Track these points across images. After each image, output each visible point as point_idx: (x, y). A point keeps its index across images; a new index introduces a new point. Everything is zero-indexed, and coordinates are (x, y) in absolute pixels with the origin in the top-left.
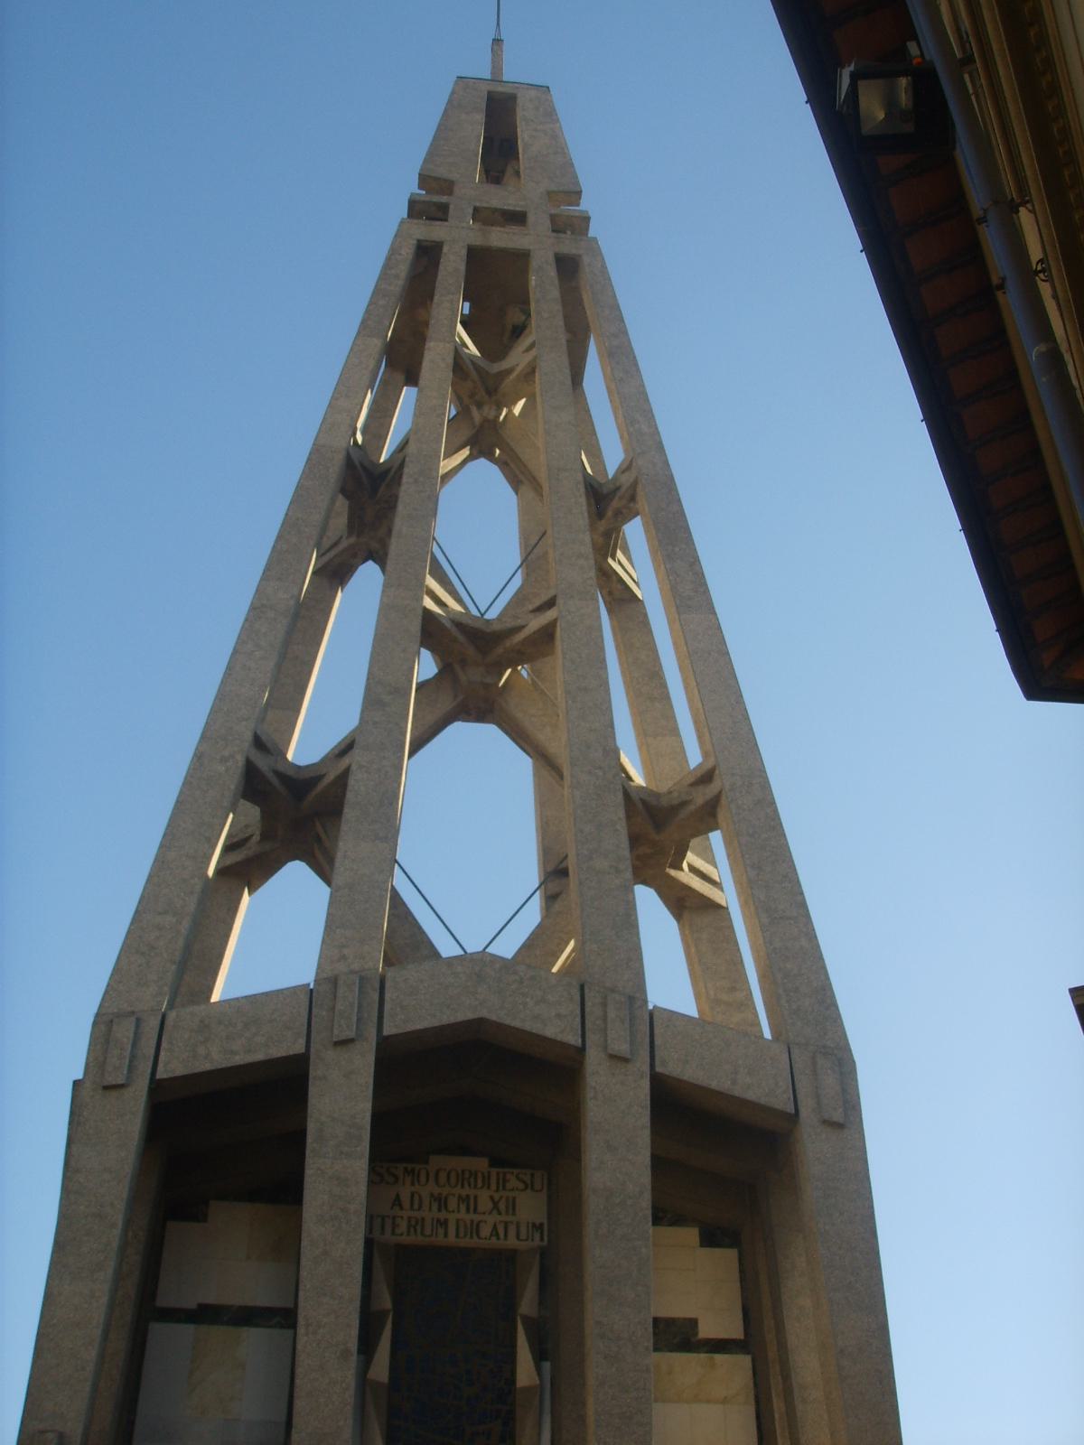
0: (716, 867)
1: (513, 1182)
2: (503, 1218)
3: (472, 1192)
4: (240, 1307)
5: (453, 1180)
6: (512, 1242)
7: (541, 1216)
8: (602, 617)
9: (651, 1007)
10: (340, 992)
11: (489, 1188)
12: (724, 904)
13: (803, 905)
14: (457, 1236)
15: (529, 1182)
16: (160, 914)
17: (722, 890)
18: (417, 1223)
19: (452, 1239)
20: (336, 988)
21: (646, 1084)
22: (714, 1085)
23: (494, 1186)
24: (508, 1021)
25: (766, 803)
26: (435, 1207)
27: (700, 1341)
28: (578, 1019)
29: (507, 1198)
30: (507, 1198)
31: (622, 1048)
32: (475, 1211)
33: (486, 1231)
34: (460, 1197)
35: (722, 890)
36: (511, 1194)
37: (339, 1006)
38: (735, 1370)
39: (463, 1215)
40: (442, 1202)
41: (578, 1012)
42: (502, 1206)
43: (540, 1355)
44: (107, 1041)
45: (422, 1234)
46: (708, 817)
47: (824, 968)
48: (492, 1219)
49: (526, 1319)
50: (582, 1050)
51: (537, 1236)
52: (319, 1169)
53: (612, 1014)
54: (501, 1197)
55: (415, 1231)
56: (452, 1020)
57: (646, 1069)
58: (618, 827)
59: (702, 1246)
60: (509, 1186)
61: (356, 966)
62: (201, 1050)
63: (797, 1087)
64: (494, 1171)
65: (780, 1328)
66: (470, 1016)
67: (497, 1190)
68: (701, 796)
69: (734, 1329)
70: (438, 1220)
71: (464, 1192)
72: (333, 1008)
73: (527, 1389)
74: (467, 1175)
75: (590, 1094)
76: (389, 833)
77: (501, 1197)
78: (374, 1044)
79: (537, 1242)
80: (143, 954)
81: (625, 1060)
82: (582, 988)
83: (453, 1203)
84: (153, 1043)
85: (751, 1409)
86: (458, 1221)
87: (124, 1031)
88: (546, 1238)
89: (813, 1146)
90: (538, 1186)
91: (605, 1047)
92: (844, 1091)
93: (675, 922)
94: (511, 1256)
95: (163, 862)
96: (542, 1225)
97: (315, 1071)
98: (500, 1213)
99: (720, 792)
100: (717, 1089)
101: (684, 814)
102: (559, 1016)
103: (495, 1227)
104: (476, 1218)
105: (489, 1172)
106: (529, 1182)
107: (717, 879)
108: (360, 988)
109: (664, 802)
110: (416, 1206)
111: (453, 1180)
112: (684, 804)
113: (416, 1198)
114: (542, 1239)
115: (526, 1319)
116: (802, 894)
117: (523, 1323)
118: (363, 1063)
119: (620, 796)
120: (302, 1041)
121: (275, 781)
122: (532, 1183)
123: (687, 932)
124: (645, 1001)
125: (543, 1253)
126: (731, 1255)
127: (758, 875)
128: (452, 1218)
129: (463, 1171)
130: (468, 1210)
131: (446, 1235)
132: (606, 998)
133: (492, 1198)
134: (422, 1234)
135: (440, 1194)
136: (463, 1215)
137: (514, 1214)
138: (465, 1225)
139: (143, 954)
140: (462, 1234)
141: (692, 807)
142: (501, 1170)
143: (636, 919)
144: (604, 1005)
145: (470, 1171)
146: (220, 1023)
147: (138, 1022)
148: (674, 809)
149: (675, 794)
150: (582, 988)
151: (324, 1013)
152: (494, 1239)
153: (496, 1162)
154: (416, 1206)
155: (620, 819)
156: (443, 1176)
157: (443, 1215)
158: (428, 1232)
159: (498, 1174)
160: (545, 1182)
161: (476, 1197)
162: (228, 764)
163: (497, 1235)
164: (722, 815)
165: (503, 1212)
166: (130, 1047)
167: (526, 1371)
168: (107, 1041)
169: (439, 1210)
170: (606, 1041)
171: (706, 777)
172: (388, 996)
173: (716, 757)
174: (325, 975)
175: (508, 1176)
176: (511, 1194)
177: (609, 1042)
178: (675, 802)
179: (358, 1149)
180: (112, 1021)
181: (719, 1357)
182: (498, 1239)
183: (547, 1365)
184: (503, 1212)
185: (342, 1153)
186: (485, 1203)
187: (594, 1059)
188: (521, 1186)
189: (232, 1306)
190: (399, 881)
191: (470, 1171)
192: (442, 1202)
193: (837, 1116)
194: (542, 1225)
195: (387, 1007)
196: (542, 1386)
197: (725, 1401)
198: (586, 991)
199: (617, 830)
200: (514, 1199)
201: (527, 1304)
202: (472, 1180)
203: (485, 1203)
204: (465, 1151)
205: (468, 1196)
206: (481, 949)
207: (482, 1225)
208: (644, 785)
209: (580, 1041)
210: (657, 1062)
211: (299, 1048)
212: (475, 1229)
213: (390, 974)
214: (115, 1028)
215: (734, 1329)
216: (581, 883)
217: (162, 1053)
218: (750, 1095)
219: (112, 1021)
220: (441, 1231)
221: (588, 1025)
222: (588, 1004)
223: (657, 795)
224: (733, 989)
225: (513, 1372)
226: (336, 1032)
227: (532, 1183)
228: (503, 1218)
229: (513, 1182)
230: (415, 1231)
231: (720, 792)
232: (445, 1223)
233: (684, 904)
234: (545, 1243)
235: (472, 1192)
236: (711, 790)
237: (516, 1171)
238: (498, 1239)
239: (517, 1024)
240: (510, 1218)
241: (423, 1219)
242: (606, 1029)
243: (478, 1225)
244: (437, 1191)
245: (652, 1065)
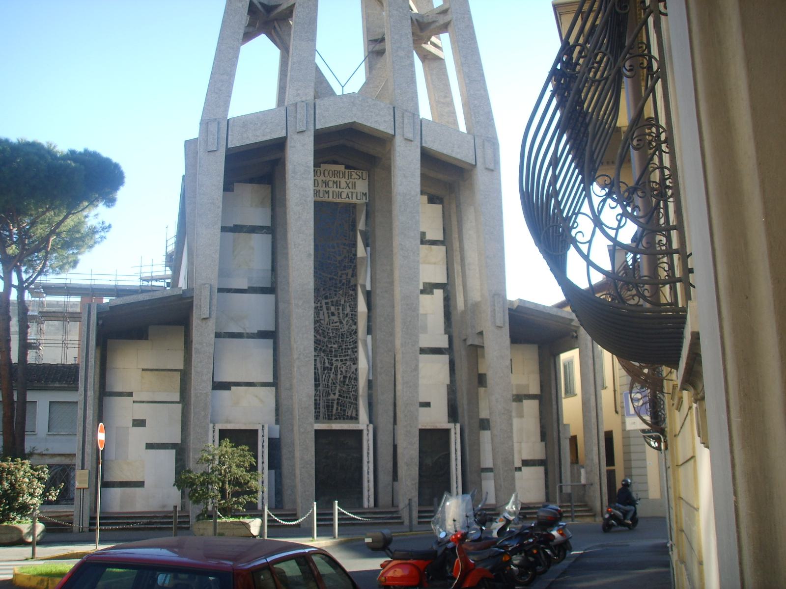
0: (440, 40)
1: (354, 176)
2: (351, 190)
3: (338, 180)
4: (250, 226)
5: (331, 175)
6: (354, 200)
7: (366, 191)
8: (631, 409)
9: (421, 118)
10: (299, 110)
11: (345, 178)
12: (443, 58)
13: (482, 75)
14: (333, 198)
15: (361, 175)
16: (221, 75)
17: (442, 51)
18: (317, 191)
19: (331, 199)
20: (296, 108)
21: (419, 151)
22: (445, 152)
23: (347, 177)
24: (365, 123)
25: (470, 26)
26: (324, 185)
27: (426, 241)
28: (393, 123)
29: (352, 182)
30: (352, 182)
31: (410, 136)
32: (340, 188)
33: (344, 196)
34: (333, 181)
35: (442, 51)
36: (354, 181)
37: (299, 116)
38: (440, 250)
39: (335, 189)
40: (326, 184)
41: (393, 120)
42: (350, 185)
43: (366, 245)
44: (207, 132)
45: (319, 197)
46: (444, 28)
47: (489, 103)
48: (346, 191)
49: (361, 232)
50: (394, 136)
51: (364, 198)
52: (295, 184)
53: (406, 121)
54: (350, 182)
55: (316, 195)
56: (343, 122)
57: (419, 145)
58: (409, 37)
59: (428, 203)
60: (353, 177)
61: (304, 99)
62: (245, 135)
63: (477, 156)
64: (347, 171)
65: (461, 241)
66: (350, 121)
67: (348, 179)
68: (442, 20)
69: (439, 236)
70: (325, 191)
71: (335, 180)
72: (296, 117)
73: (362, 258)
74: (336, 172)
75: (397, 154)
76: (312, 38)
77: (350, 182)
78: (313, 133)
79: (364, 200)
80: (217, 93)
81: (411, 141)
82: (394, 108)
83: (331, 184)
84: (225, 132)
85: (445, 267)
86: (333, 191)
87: (213, 128)
88: (368, 199)
89: (481, 177)
90: (364, 178)
91: (403, 136)
92: (494, 156)
93: (421, 63)
94: (354, 206)
95: (220, 51)
96: (366, 193)
97: (289, 144)
98: (350, 188)
99: (451, 21)
100: (446, 154)
101: (433, 26)
102: (385, 121)
103: (348, 195)
104: (340, 190)
105: (345, 171)
106: (361, 175)
107: (440, 45)
108: (306, 108)
109: (425, 20)
110: (316, 185)
111: (331, 175)
112: (434, 22)
113: (316, 181)
114: (366, 199)
115: (361, 232)
116: (482, 70)
117: (360, 233)
118: (309, 141)
119: (410, 21)
120: (285, 131)
121: (259, 6)
122: (362, 176)
123: (427, 69)
124: (419, 116)
125: (367, 204)
126: (441, 206)
127: (465, 61)
128: (331, 190)
129: (334, 171)
130: (337, 187)
131: (328, 197)
132: (403, 114)
133: (346, 182)
134: (319, 197)
135: (326, 180)
136: (335, 189)
137: (355, 189)
138: (336, 193)
139: (217, 93)
140: (335, 197)
141: (437, 24)
142: (350, 170)
143: (415, 80)
144: (403, 117)
145: (337, 171)
146: (251, 123)
147: (218, 123)
148: (429, 24)
149: (430, 17)
150: (394, 108)
151: (292, 119)
152: (347, 199)
153: (347, 167)
154: (316, 185)
155: (409, 32)
156: (326, 174)
157: (327, 189)
158: (321, 196)
159: (348, 172)
160: (367, 176)
161: (340, 182)
162: (243, 3)
163: (349, 197)
164: (450, 29)
165: (351, 188)
166: (216, 134)
167: (361, 251)
168: (207, 132)
169: (326, 187)
170: (404, 132)
171: (444, 12)
172: (317, 112)
173: (450, 4)
174: (291, 103)
175: (353, 173)
176: (354, 181)
177: (405, 133)
178: (430, 21)
179: (309, 176)
180: (208, 123)
181: (433, 247)
182: (349, 199)
183: (369, 249)
184: (351, 188)
185: (303, 178)
186: (343, 185)
187: (398, 140)
188: (358, 177)
189: (247, 225)
190: (318, 61)
191: (337, 171)
192: (326, 184)
193: (492, 167)
194: (366, 193)
195: (317, 116)
196: (367, 257)
197: (435, 264)
198: (396, 110)
199: (408, 38)
200: (355, 183)
201: (361, 226)
202: (338, 174)
203: (343, 185)
204: (335, 162)
205: (337, 181)
206: (317, 49)
207: (342, 193)
208: (417, 12)
209: (393, 132)
210: (423, 142)
211: (283, 134)
212: (340, 195)
213: (318, 101)
214: (209, 126)
215: (439, 236)
216: (393, 62)
217: (229, 137)
218: (458, 157)
219: (208, 123)
220: (327, 195)
221: (397, 125)
222: (396, 116)
223: (422, 17)
224: (445, 97)
225: (356, 251)
226: (297, 128)
227: (362, 176)
228: (351, 190)
229: (354, 176)
230: (316, 195)
231: (451, 21)
232: (328, 192)
233: (427, 57)
234: (367, 201)
235: (338, 180)
236: (447, 18)
237: (355, 171)
238: (349, 199)
239: (369, 124)
240: (353, 191)
241: (319, 190)
242: (403, 128)
243: (341, 193)
244: (324, 179)
245: (421, 144)
